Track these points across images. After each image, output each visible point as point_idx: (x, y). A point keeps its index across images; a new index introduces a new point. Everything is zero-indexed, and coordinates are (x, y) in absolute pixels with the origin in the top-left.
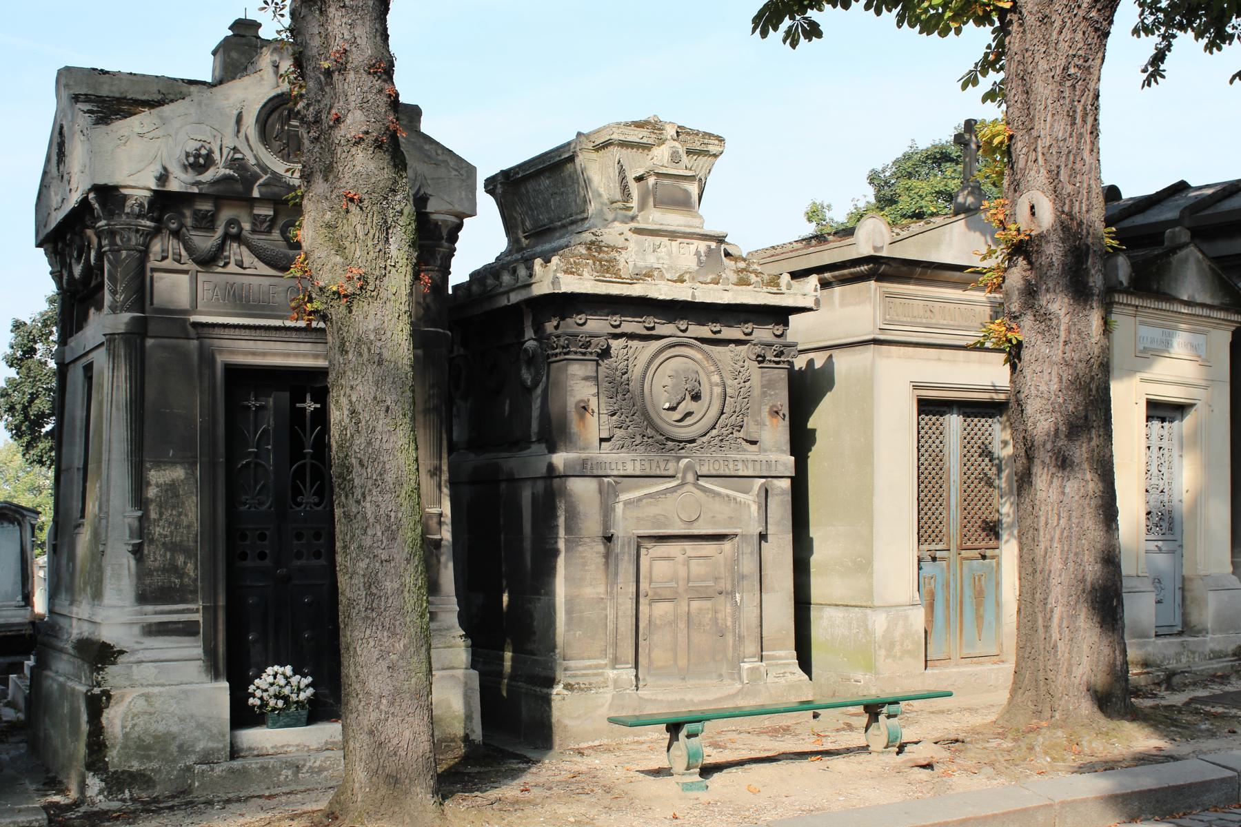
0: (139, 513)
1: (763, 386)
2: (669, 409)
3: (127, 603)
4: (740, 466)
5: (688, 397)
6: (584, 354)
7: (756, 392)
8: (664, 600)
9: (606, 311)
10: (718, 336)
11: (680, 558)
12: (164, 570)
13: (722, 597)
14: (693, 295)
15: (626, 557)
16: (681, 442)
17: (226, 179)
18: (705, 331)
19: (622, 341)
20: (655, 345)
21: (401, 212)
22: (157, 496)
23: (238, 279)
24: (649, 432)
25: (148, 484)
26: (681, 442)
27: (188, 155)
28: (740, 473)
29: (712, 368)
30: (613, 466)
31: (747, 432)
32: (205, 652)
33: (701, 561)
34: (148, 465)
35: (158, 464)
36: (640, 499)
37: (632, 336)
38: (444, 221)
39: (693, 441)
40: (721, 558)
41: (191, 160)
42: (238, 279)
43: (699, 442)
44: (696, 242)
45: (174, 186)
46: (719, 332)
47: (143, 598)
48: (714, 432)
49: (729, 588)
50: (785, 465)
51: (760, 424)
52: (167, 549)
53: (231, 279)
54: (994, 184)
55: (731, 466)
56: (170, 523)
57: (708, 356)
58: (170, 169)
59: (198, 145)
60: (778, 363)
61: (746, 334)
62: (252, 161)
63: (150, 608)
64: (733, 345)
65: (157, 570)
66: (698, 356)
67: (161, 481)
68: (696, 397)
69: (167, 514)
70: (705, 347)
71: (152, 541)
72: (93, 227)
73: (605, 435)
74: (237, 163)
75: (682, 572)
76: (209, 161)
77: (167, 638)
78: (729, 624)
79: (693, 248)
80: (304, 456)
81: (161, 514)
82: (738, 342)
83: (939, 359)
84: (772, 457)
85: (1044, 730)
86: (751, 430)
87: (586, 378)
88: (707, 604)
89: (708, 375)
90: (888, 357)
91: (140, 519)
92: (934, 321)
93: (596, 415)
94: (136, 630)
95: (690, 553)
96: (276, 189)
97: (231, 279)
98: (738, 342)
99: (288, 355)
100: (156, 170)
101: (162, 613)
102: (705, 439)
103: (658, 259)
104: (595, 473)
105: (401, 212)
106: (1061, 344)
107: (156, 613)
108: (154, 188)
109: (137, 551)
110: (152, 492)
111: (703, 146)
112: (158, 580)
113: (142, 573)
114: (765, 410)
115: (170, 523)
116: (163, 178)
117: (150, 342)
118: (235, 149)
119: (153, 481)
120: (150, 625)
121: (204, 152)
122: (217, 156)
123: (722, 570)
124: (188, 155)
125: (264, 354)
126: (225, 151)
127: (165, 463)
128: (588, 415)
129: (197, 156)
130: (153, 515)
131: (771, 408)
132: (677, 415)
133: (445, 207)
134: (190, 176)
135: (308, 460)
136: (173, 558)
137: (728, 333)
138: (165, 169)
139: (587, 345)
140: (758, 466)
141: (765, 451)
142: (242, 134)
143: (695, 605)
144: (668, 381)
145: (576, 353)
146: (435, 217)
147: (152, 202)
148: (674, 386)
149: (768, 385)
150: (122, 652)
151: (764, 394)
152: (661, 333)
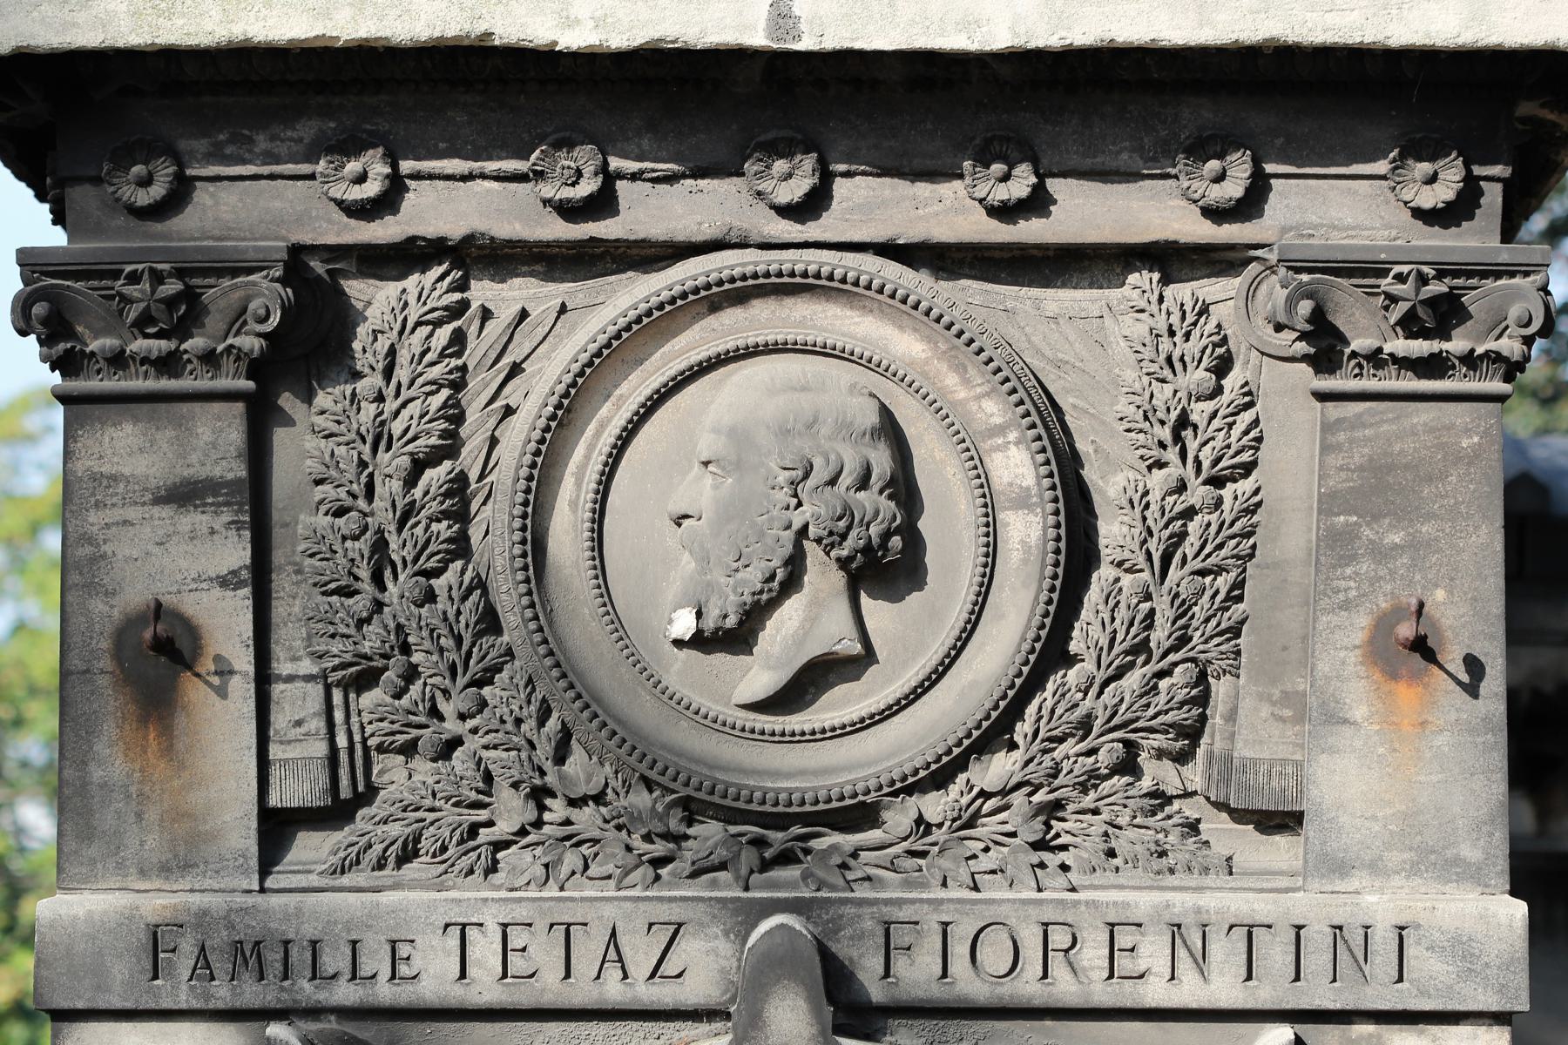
1: (1329, 503)
2: (701, 642)
5: (823, 576)
6: (168, 364)
7: (1290, 534)
9: (307, 130)
10: (1030, 231)
16: (780, 821)
18: (951, 209)
19: (425, 287)
20: (633, 292)
21: (1287, 206)
26: (780, 821)
28: (1156, 993)
31: (1225, 766)
37: (478, 256)
39: (860, 815)
43: (898, 818)
46: (1038, 203)
48: (999, 768)
50: (1461, 949)
51: (1313, 714)
54: (406, 649)
60: (1433, 366)
61: (1215, 214)
64: (1142, 280)
66: (906, 345)
68: (888, 567)
72: (1041, 177)
73: (296, 788)
82: (1170, 260)
84: (1378, 904)
86: (1248, 727)
87: (184, 495)
93: (242, 689)
98: (1170, 260)
102: (935, 805)
105: (1287, 206)
114: (1344, 639)
128: (195, 691)
131: (1383, 625)
132: (759, 674)
137: (1084, 211)
139: (184, 314)
140: (1275, 953)
141: (1339, 867)
144: (701, 492)
145: (118, 361)
149: (1367, 498)
151: (1336, 546)
152: (656, 229)
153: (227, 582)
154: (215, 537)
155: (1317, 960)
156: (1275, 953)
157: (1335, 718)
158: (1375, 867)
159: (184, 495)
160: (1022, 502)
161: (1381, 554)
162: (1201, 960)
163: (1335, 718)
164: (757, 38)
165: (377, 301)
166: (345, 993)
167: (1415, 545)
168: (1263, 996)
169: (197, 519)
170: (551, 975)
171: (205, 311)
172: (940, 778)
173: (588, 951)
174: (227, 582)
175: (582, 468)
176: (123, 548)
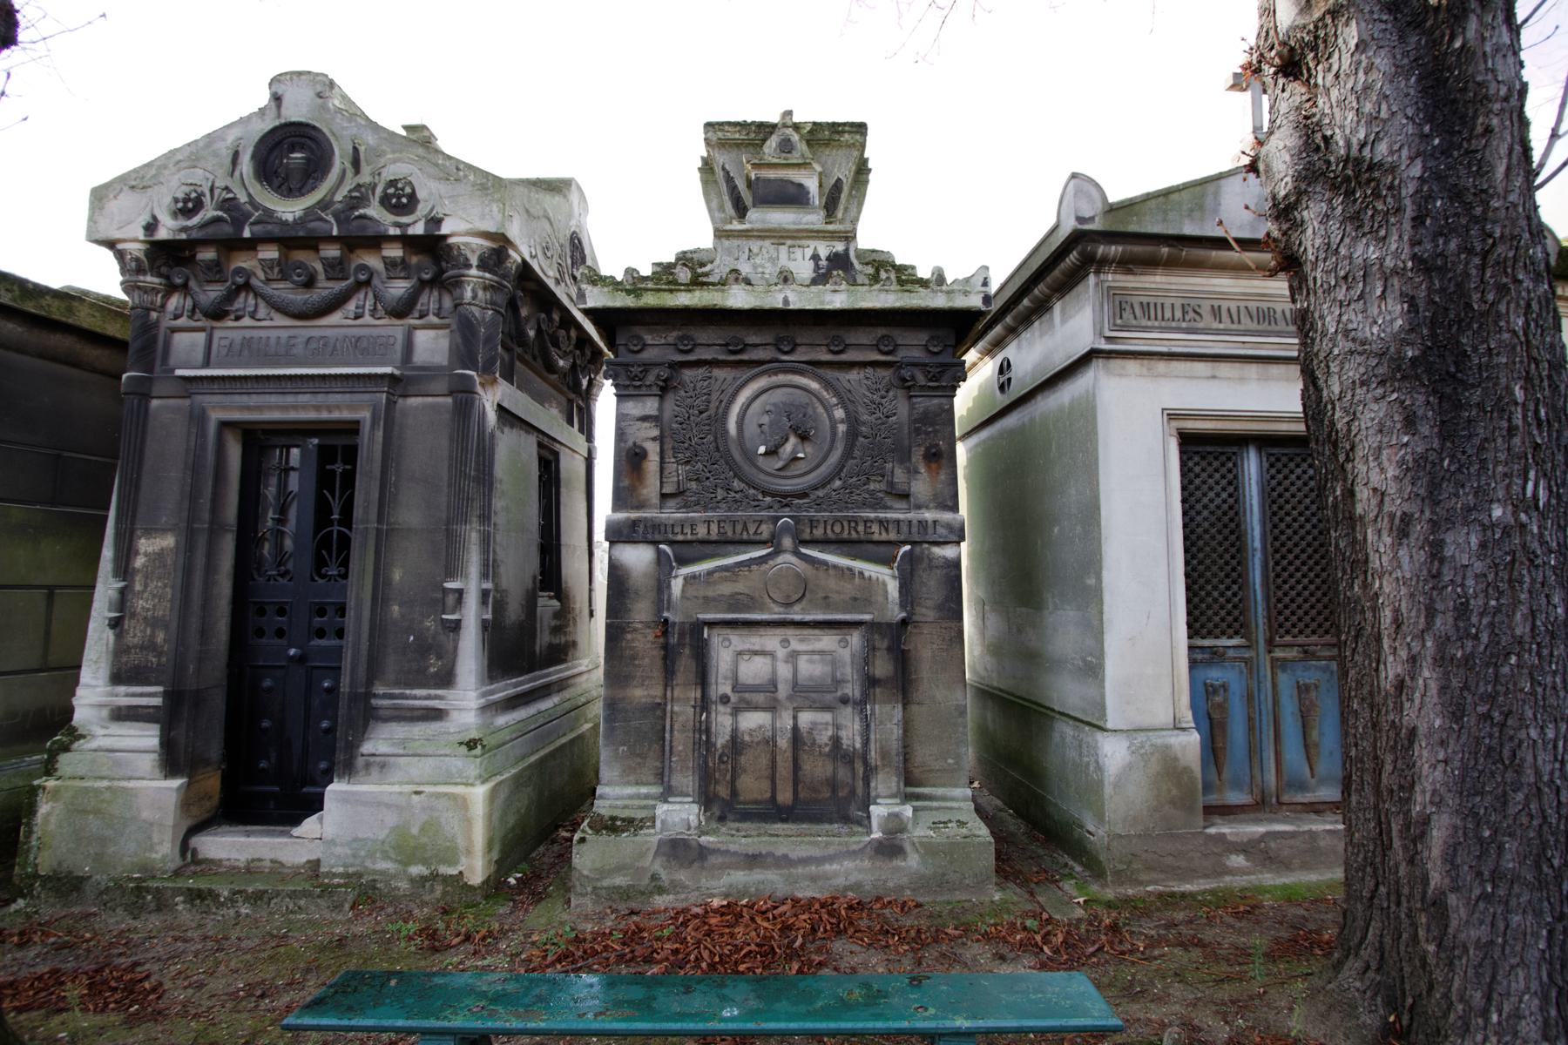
0: (122, 584)
2: (766, 454)
3: (101, 682)
4: (875, 528)
8: (756, 708)
11: (781, 653)
12: (142, 648)
13: (849, 710)
14: (786, 301)
15: (687, 651)
16: (785, 497)
17: (217, 220)
22: (144, 566)
23: (256, 334)
24: (736, 484)
25: (137, 553)
26: (785, 497)
27: (176, 200)
28: (876, 537)
29: (834, 401)
30: (678, 529)
32: (162, 744)
33: (816, 657)
34: (139, 533)
35: (149, 532)
36: (710, 573)
38: (466, 244)
39: (804, 495)
40: (845, 654)
41: (180, 205)
42: (256, 334)
44: (813, 244)
45: (163, 234)
47: (117, 678)
49: (857, 694)
51: (912, 472)
52: (147, 625)
53: (248, 334)
55: (861, 528)
56: (154, 596)
57: (827, 385)
58: (160, 217)
59: (187, 189)
62: (243, 198)
63: (122, 689)
65: (135, 647)
66: (814, 385)
67: (150, 549)
69: (152, 586)
70: (830, 374)
71: (133, 615)
73: (668, 489)
74: (229, 204)
75: (784, 671)
76: (198, 204)
77: (141, 724)
78: (858, 746)
79: (809, 252)
80: (331, 523)
81: (146, 586)
83: (1214, 377)
85: (1435, 817)
88: (827, 717)
89: (828, 409)
90: (1120, 375)
91: (123, 592)
92: (1201, 325)
94: (105, 713)
95: (795, 645)
96: (270, 227)
97: (248, 334)
99: (295, 408)
100: (145, 218)
101: (134, 695)
102: (820, 493)
103: (755, 267)
104: (650, 537)
106: (1407, 225)
107: (127, 695)
108: (142, 237)
109: (115, 624)
110: (139, 562)
111: (842, 138)
112: (134, 658)
113: (120, 650)
115: (154, 596)
116: (151, 227)
117: (155, 403)
118: (227, 189)
119: (142, 550)
120: (119, 708)
121: (193, 195)
122: (207, 200)
123: (848, 670)
124: (176, 200)
125: (259, 408)
126: (217, 192)
127: (156, 530)
129: (186, 200)
130: (138, 587)
131: (927, 449)
133: (463, 226)
134: (183, 222)
135: (336, 528)
136: (153, 635)
138: (154, 218)
140: (905, 529)
142: (237, 173)
143: (806, 718)
146: (451, 240)
147: (147, 253)
148: (771, 424)
150: (83, 737)
153: (654, 439)
154: (1252, 176)
155: (914, 530)
156: (905, 529)
157: (917, 472)
158: (927, 508)
159: (644, 419)
160: (842, 422)
161: (927, 433)
162: (887, 530)
163: (917, 472)
164: (780, 306)
165: (688, 374)
166: (680, 537)
167: (935, 432)
168: (902, 538)
169: (646, 424)
170: (730, 534)
171: (417, 201)
172: (824, 486)
173: (739, 528)
174: (654, 439)
175: (317, 408)
176: (629, 431)
